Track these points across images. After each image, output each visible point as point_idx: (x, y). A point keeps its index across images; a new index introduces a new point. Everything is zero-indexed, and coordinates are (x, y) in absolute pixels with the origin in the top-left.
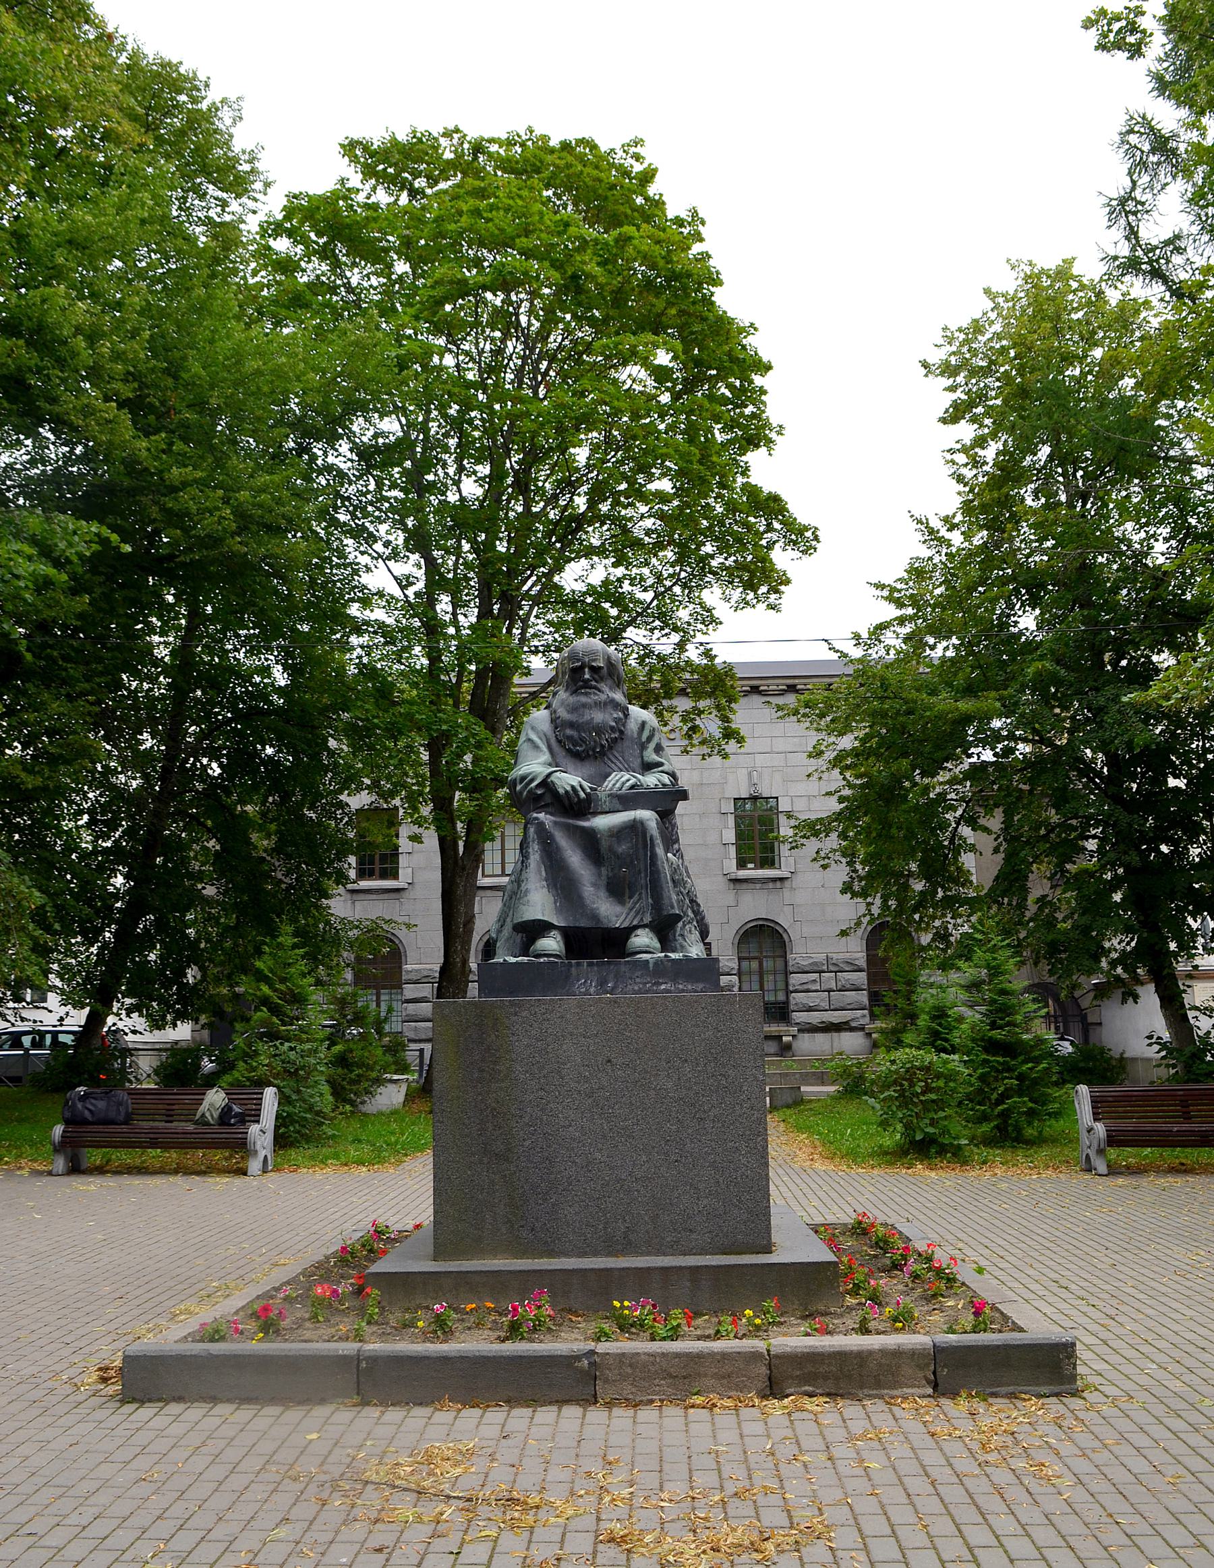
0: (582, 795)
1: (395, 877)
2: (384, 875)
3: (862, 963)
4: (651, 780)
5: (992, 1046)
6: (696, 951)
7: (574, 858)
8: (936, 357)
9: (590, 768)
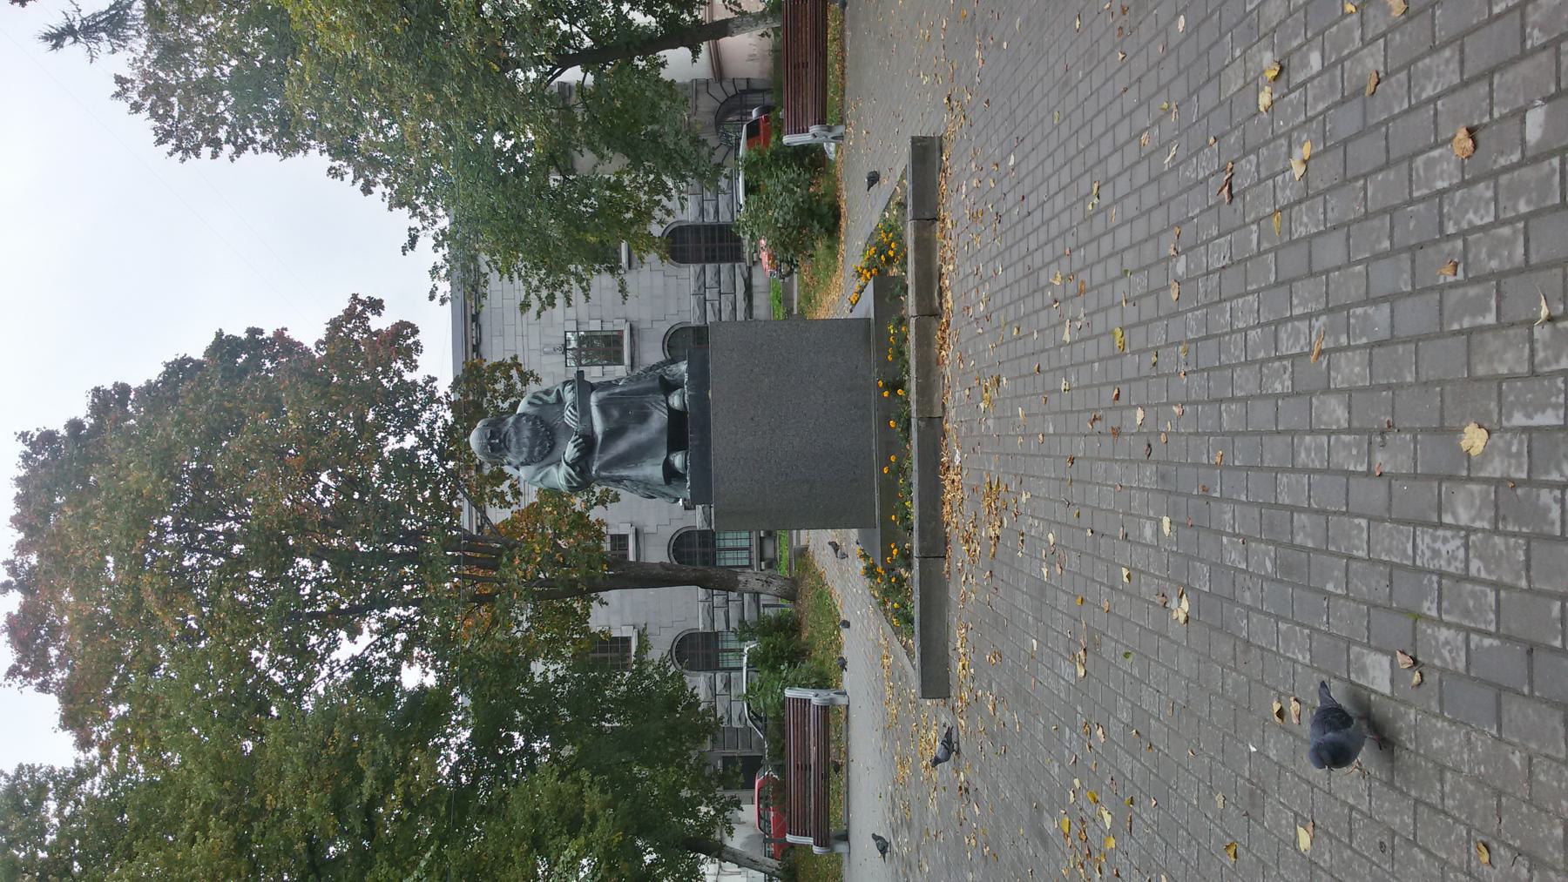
1: (627, 640)
3: (698, 267)
4: (569, 396)
7: (622, 446)
9: (561, 440)
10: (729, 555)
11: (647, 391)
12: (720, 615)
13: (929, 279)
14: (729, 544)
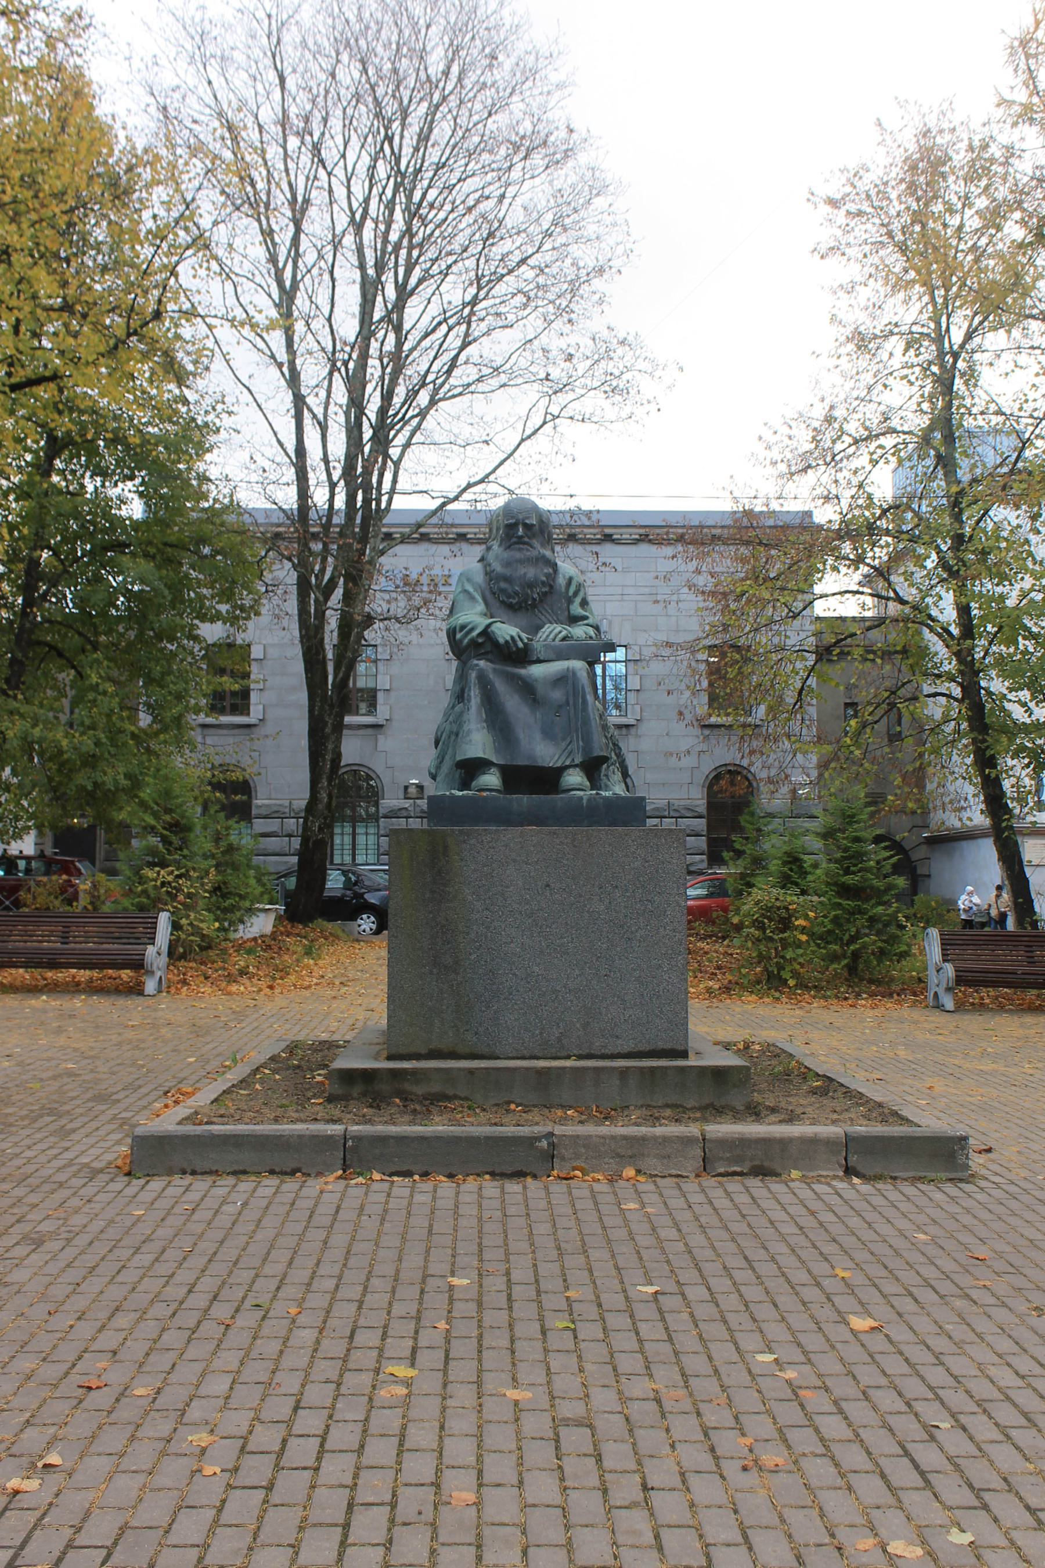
0: (520, 645)
2: (235, 710)
4: (579, 631)
5: (845, 891)
6: (619, 790)
10: (348, 839)
11: (587, 738)
12: (273, 825)
13: (762, 1163)
14: (361, 840)
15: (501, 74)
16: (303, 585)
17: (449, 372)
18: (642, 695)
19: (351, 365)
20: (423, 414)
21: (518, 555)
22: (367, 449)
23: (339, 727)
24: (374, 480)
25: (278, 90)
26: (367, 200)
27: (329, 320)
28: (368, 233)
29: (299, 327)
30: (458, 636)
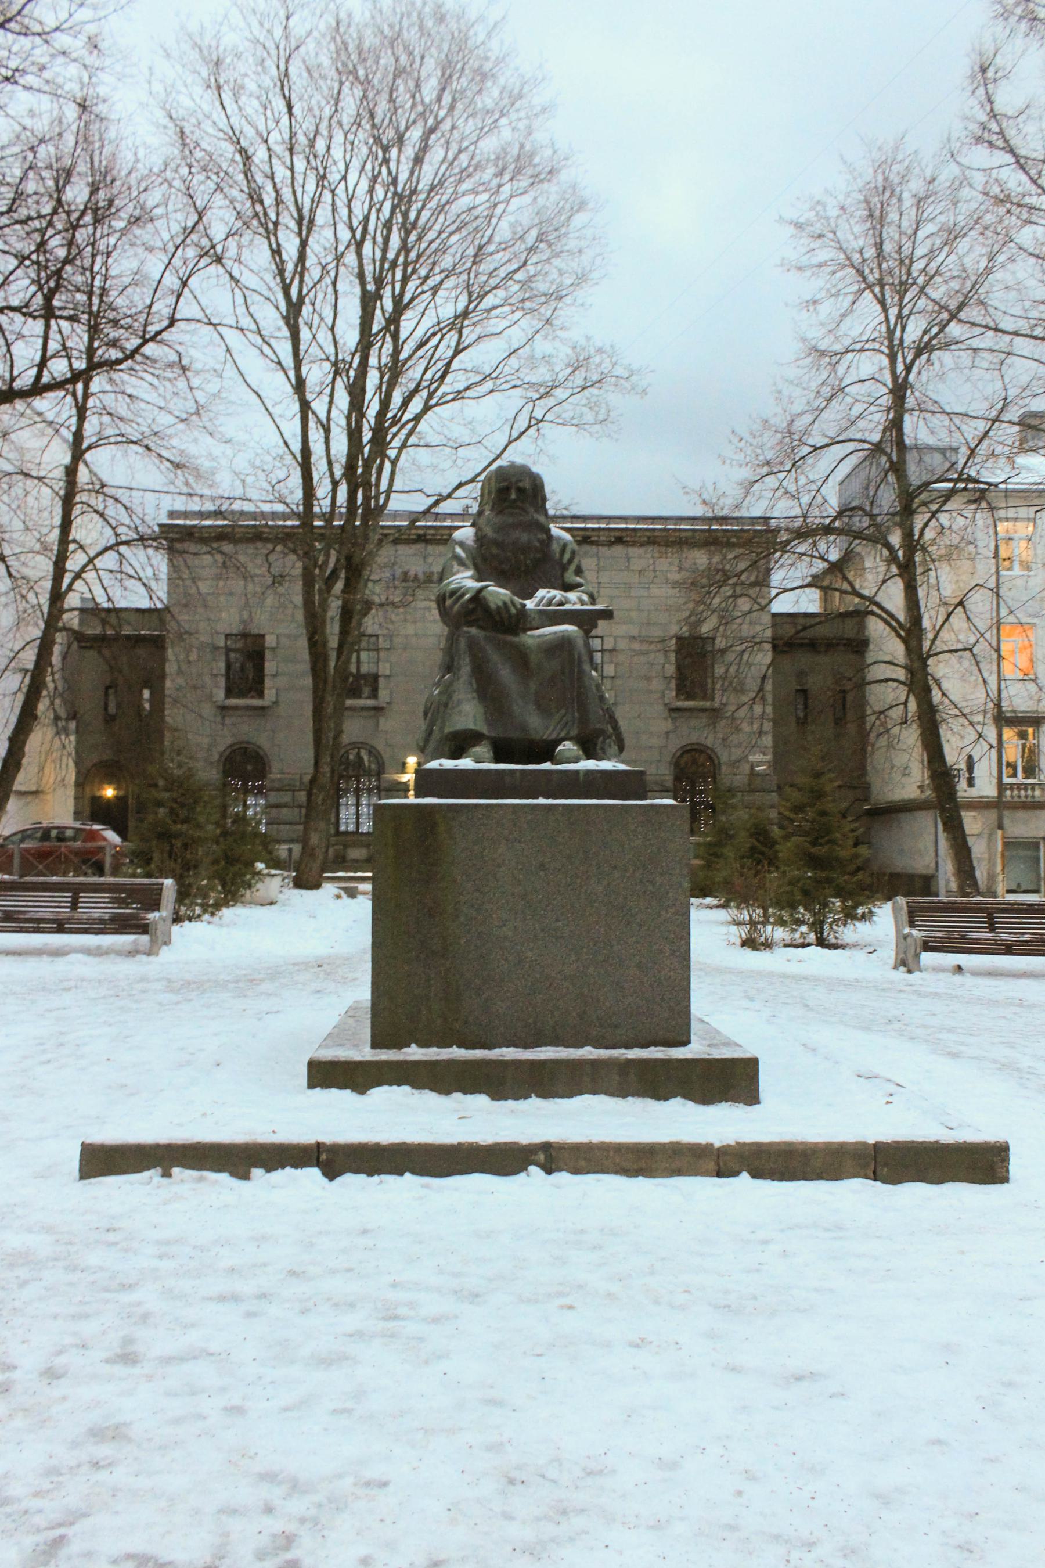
0: (513, 611)
7: (506, 674)
8: (791, 214)
10: (353, 810)
12: (286, 798)
15: (488, 100)
16: (308, 580)
17: (443, 377)
18: (618, 682)
19: (352, 373)
20: (417, 419)
21: (510, 520)
22: (367, 450)
23: (340, 710)
24: (373, 479)
25: (287, 117)
26: (367, 218)
27: (332, 329)
28: (367, 248)
29: (305, 334)
30: (448, 602)
